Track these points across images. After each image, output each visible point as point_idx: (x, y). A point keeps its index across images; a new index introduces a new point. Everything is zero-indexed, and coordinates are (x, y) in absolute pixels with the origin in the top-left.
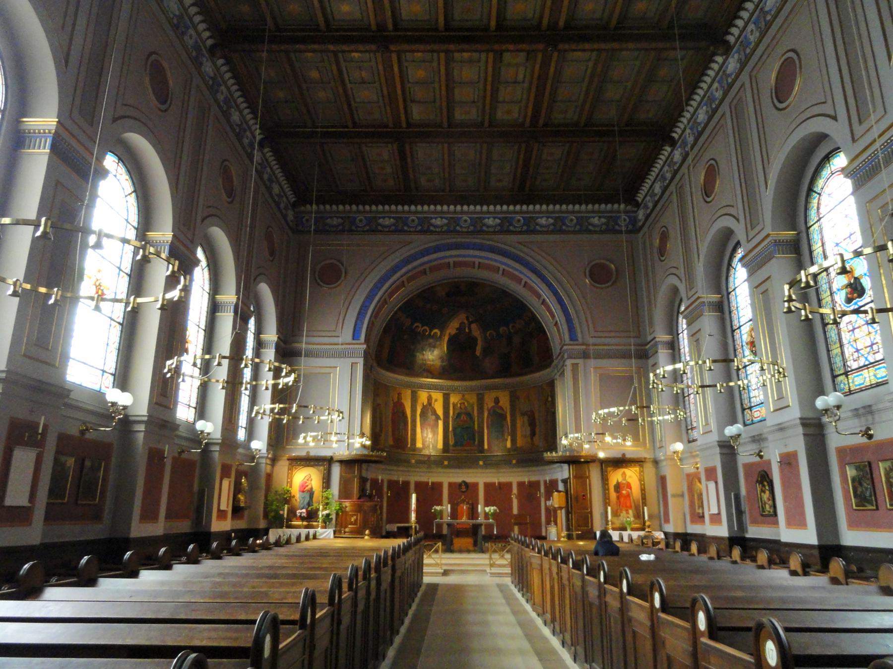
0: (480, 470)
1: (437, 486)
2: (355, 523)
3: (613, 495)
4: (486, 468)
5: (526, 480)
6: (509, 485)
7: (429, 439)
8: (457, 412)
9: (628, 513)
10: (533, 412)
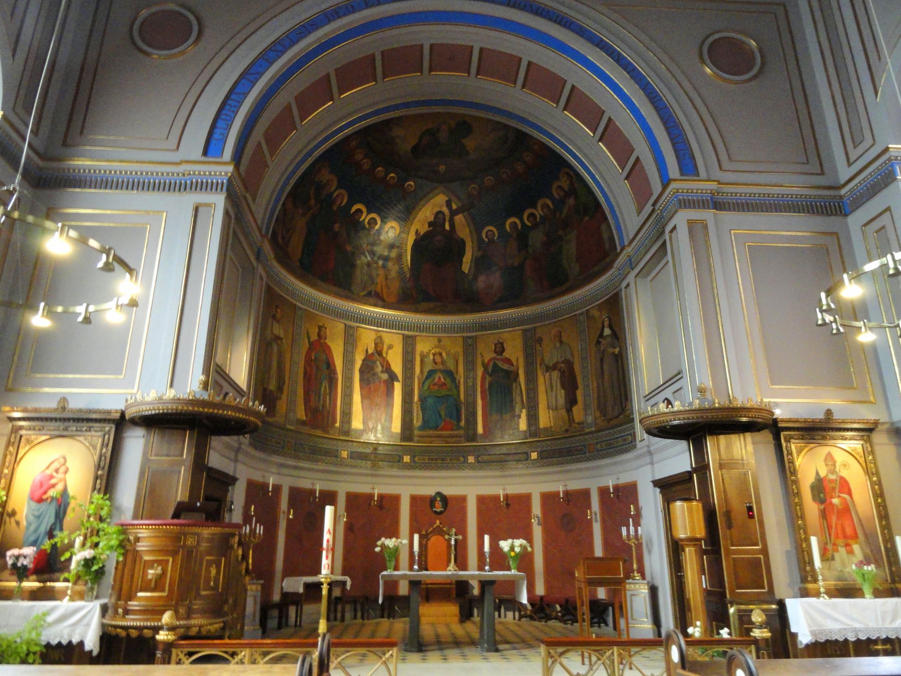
0: (471, 473)
1: (389, 504)
2: (158, 585)
3: (812, 508)
4: (481, 468)
5: (561, 489)
6: (526, 499)
7: (375, 422)
8: (426, 370)
9: (851, 552)
10: (570, 364)
